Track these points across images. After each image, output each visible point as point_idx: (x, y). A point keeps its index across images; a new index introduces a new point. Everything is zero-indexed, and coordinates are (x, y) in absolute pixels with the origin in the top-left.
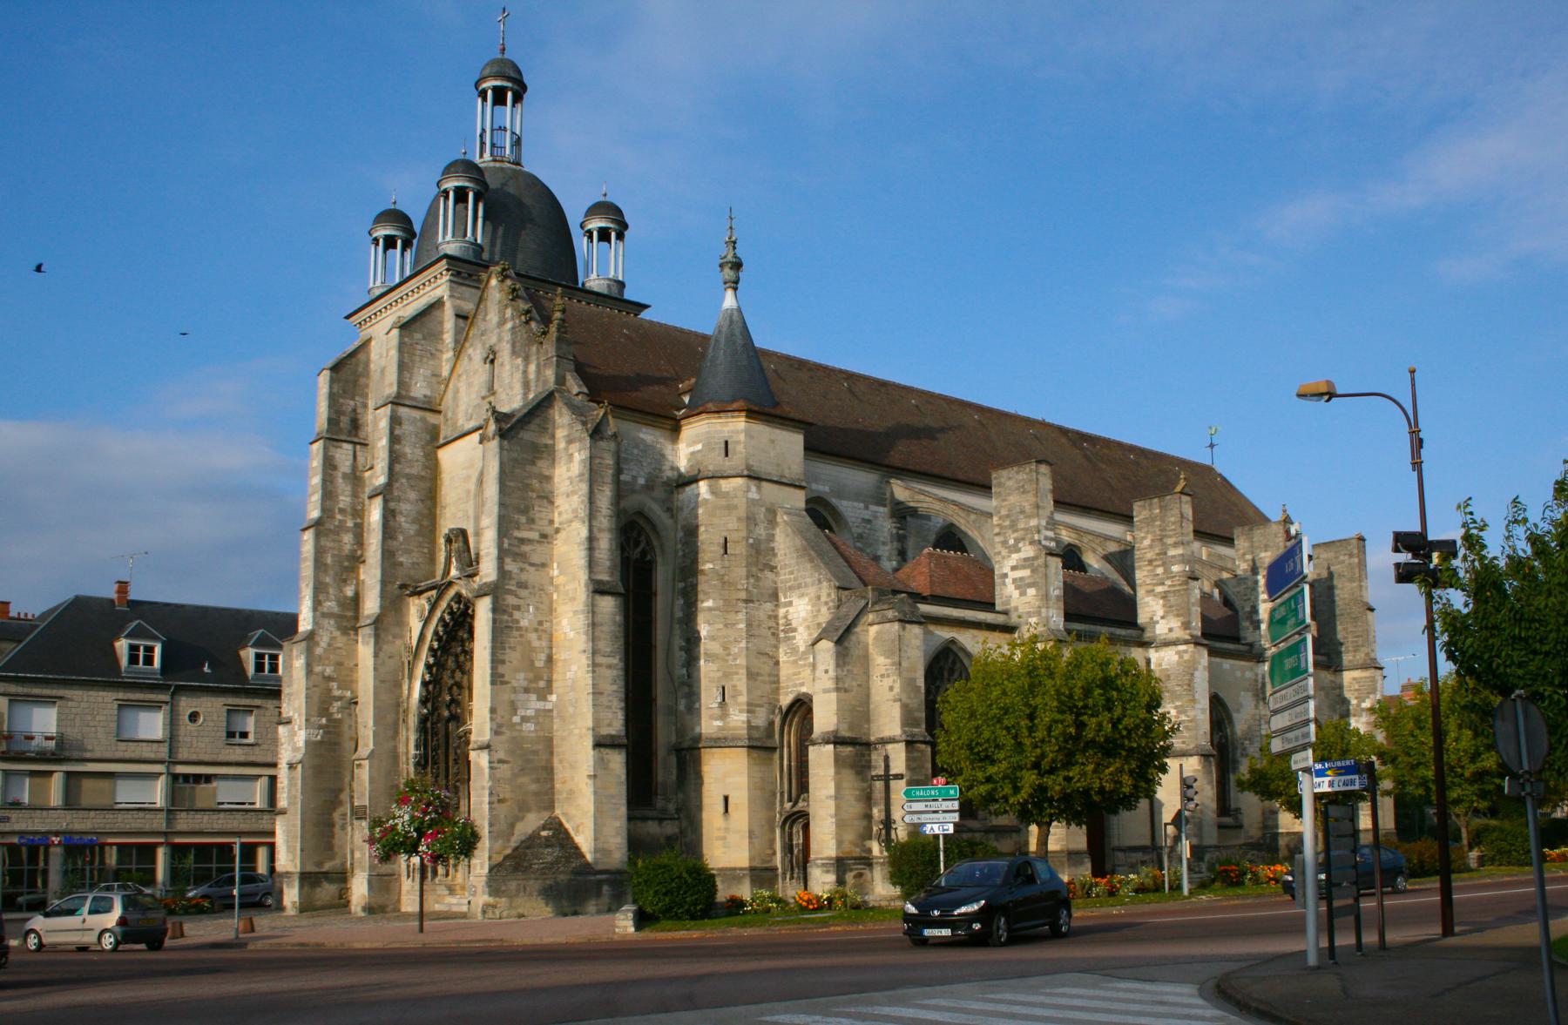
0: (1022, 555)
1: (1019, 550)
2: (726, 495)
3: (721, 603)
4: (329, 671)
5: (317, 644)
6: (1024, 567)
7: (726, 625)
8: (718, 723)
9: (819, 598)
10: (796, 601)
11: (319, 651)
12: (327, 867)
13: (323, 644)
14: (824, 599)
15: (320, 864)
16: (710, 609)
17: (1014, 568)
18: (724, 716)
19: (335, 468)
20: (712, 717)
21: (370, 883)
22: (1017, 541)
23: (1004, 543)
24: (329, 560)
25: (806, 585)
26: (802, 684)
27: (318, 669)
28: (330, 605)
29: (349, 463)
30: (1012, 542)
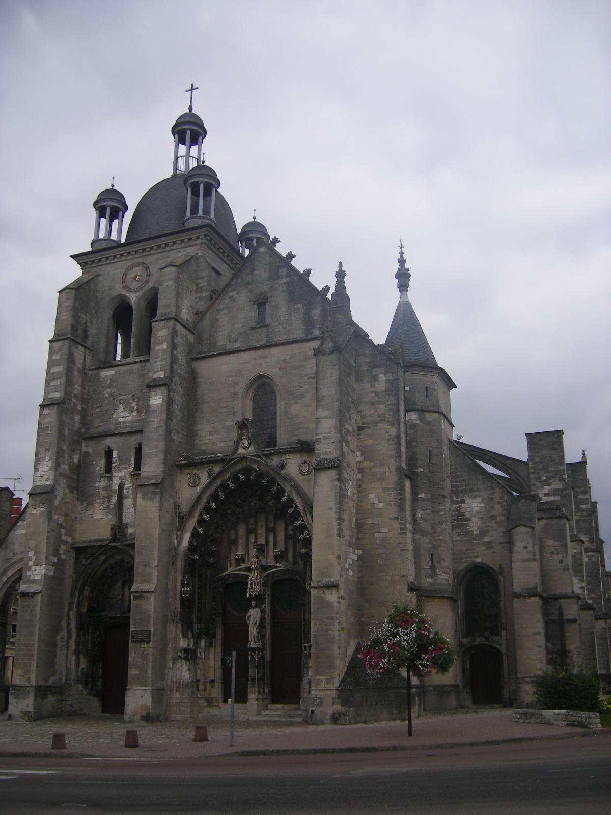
0: (553, 487)
1: (550, 484)
2: (429, 423)
3: (429, 496)
4: (61, 519)
5: (56, 497)
6: (555, 495)
7: (433, 512)
8: (430, 580)
9: (492, 499)
10: (468, 500)
11: (56, 502)
12: (51, 681)
13: (59, 498)
14: (497, 499)
15: (46, 679)
16: (422, 499)
17: (546, 495)
18: (433, 575)
19: (74, 363)
20: (427, 576)
21: (153, 696)
22: (548, 478)
23: (538, 479)
24: (66, 433)
25: (478, 490)
26: (477, 557)
27: (55, 517)
28: (65, 467)
29: (81, 361)
30: (544, 478)
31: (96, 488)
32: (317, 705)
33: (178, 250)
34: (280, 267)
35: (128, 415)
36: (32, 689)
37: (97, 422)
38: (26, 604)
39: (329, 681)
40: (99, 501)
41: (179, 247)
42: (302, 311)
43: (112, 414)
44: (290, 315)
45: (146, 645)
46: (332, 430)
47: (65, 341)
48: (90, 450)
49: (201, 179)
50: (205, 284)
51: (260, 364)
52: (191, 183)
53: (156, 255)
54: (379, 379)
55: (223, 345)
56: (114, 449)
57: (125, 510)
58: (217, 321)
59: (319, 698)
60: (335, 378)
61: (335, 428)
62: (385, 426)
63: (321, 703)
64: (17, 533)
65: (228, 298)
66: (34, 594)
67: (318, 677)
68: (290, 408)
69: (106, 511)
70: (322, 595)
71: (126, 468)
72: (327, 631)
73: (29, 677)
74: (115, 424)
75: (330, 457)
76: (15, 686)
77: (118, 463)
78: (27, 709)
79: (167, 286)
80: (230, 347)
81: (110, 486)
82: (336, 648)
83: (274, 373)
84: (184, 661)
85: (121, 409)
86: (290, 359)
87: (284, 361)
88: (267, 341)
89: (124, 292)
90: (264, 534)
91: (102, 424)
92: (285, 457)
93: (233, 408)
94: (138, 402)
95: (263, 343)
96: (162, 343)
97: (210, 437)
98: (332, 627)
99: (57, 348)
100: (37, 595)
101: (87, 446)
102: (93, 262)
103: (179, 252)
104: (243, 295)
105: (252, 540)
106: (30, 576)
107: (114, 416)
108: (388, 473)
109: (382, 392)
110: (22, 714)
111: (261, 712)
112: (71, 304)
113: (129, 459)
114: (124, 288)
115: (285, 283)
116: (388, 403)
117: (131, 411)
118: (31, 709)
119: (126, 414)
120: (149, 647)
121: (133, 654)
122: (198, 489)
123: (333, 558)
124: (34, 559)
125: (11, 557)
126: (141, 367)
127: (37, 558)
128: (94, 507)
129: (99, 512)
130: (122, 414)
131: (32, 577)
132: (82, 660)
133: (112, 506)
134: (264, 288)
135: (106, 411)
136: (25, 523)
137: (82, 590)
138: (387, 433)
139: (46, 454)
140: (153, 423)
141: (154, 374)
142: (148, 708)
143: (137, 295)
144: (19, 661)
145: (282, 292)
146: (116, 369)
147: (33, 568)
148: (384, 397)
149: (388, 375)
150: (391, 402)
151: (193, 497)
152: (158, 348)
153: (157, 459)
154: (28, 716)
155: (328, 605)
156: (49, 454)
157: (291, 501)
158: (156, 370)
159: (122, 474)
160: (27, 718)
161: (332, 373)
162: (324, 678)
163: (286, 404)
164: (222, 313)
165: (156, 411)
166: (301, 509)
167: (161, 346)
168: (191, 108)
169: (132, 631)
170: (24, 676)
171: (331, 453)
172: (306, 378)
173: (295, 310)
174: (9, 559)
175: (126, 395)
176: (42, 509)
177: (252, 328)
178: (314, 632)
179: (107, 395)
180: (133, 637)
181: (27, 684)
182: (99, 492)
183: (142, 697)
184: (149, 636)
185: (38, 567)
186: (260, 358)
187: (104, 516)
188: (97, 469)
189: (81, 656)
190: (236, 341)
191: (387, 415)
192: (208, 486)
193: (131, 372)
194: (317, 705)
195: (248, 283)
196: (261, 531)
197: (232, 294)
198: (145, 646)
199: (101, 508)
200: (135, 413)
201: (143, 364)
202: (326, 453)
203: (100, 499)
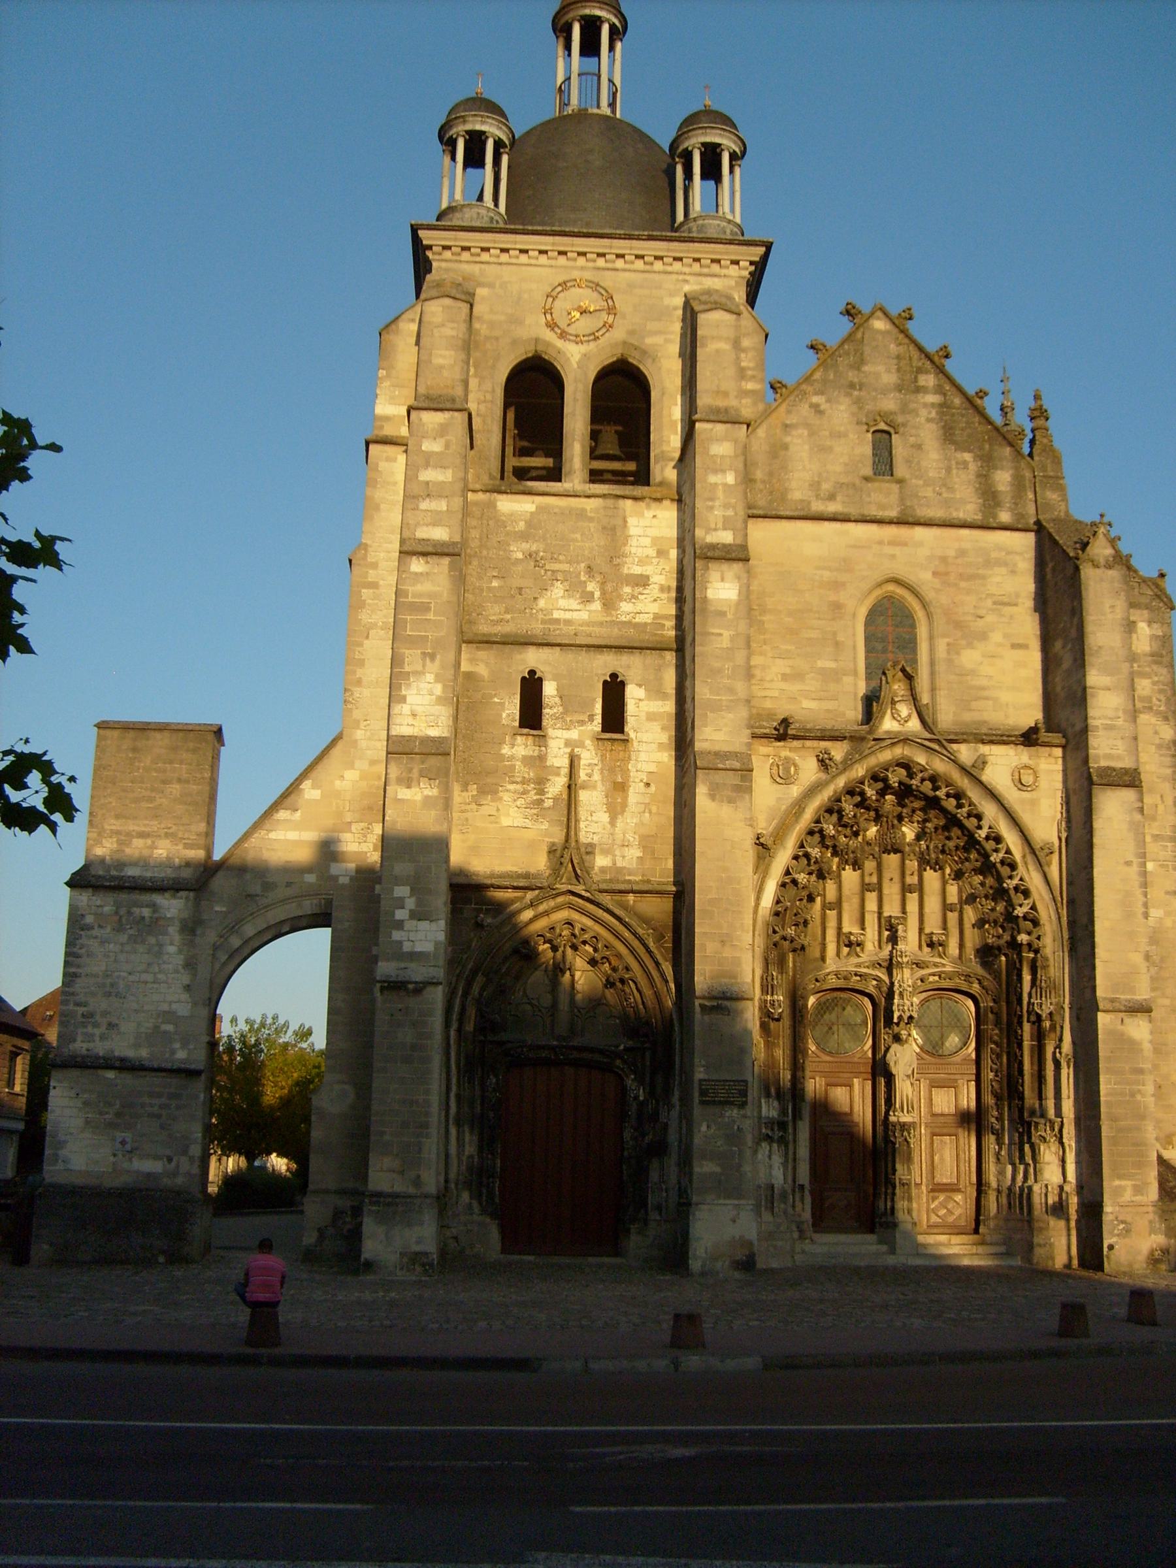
31: (502, 758)
32: (1118, 1235)
33: (681, 277)
34: (919, 371)
35: (578, 607)
36: (428, 1201)
37: (494, 611)
38: (400, 1006)
39: (1138, 1190)
40: (512, 787)
41: (687, 270)
42: (973, 467)
43: (535, 599)
44: (949, 470)
45: (735, 1111)
46: (1120, 714)
47: (456, 414)
48: (482, 670)
50: (751, 365)
51: (893, 556)
52: (703, 144)
53: (627, 274)
54: (1139, 631)
55: (802, 501)
56: (627, 679)
57: (583, 814)
58: (785, 447)
59: (1122, 1222)
60: (1119, 616)
61: (1125, 711)
62: (1153, 720)
63: (1128, 1231)
64: (273, 835)
65: (807, 406)
66: (420, 988)
67: (1117, 1183)
68: (958, 653)
69: (535, 811)
70: (1120, 1027)
71: (582, 723)
72: (1133, 1095)
73: (419, 1177)
74: (544, 622)
75: (1118, 765)
76: (379, 1194)
77: (561, 709)
79: (717, 351)
80: (817, 507)
81: (542, 758)
82: (1150, 1128)
83: (924, 578)
84: (775, 1145)
85: (558, 590)
86: (956, 558)
87: (944, 559)
88: (902, 512)
89: (549, 336)
90: (897, 898)
91: (508, 617)
92: (985, 749)
93: (835, 634)
94: (603, 584)
95: (893, 513)
96: (723, 471)
97: (783, 685)
98: (1141, 1087)
99: (430, 426)
100: (430, 989)
101: (471, 660)
103: (686, 281)
104: (842, 408)
105: (871, 905)
106: (400, 943)
107: (542, 603)
108: (1161, 808)
109: (1145, 655)
110: (405, 1260)
111: (355, 1236)
112: (461, 336)
113: (588, 704)
114: (548, 325)
115: (933, 405)
116: (1156, 679)
117: (588, 598)
118: (431, 1247)
119: (573, 604)
120: (745, 1116)
121: (704, 1128)
122: (795, 791)
123: (1137, 958)
124: (411, 903)
126: (605, 508)
127: (419, 903)
128: (501, 799)
129: (513, 811)
130: (562, 603)
131: (407, 947)
132: (467, 1137)
133: (549, 803)
134: (889, 404)
135: (521, 589)
136: (298, 814)
137: (469, 984)
138: (1156, 733)
139: (424, 666)
140: (719, 638)
141: (707, 533)
142: (751, 1243)
143: (583, 348)
144: (387, 1138)
145: (929, 420)
146: (539, 499)
147: (409, 925)
148: (1149, 666)
149: (1155, 626)
150: (1162, 678)
151: (784, 807)
152: (713, 479)
153: (731, 716)
154: (423, 1265)
155: (1132, 1046)
156: (433, 667)
158: (713, 526)
159: (574, 734)
160: (418, 1268)
161: (1113, 607)
162: (1129, 1183)
163: (948, 644)
164: (794, 433)
165: (723, 614)
166: (1017, 855)
167: (719, 476)
169: (700, 1080)
170: (402, 1173)
171: (1119, 757)
172: (989, 603)
173: (957, 463)
174: (251, 897)
175: (569, 562)
176: (428, 792)
177: (866, 479)
178: (1106, 1095)
179: (520, 556)
180: (703, 1093)
181: (412, 1190)
182: (513, 767)
183: (734, 1221)
184: (744, 1093)
185: (424, 925)
186: (893, 543)
187: (528, 823)
188: (504, 715)
189: (466, 1129)
190: (832, 497)
191: (1154, 699)
192: (813, 790)
193: (581, 514)
194: (1118, 1235)
195: (852, 386)
196: (892, 890)
197: (815, 399)
198: (734, 1112)
199: (518, 803)
200: (597, 606)
201: (610, 502)
202: (1108, 757)
203: (517, 783)
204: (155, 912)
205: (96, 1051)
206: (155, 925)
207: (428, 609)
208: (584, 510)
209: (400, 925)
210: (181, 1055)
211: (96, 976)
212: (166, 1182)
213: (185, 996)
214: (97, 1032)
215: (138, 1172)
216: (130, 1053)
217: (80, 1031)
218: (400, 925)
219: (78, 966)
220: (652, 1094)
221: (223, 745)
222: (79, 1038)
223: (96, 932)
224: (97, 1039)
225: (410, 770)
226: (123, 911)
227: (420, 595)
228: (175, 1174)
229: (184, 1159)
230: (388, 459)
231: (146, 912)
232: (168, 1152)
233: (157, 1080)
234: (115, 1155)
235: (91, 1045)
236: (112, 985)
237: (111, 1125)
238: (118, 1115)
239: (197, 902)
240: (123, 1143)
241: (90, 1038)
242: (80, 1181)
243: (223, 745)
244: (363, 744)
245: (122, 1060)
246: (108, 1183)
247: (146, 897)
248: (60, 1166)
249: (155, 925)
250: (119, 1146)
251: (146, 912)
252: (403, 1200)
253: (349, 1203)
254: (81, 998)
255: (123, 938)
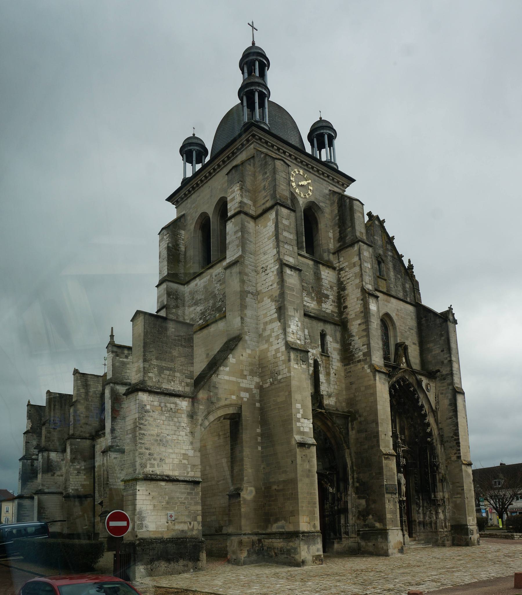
49: (325, 131)
76: (303, 533)
78: (317, 554)
102: (266, 142)
125: (216, 401)
144: (304, 508)
157: (422, 406)
168: (253, 43)
180: (387, 489)
181: (313, 530)
204: (176, 406)
205: (156, 472)
206: (175, 412)
207: (294, 291)
208: (308, 264)
209: (298, 420)
210: (191, 474)
211: (152, 435)
212: (189, 534)
213: (190, 447)
214: (156, 463)
215: (177, 530)
216: (170, 473)
217: (148, 462)
218: (298, 420)
219: (145, 430)
220: (338, 490)
221: (457, 324)
222: (148, 466)
223: (151, 414)
224: (156, 466)
225: (297, 356)
226: (162, 405)
227: (291, 284)
228: (192, 529)
229: (195, 523)
230: (247, 222)
231: (172, 406)
232: (189, 520)
233: (182, 486)
234: (167, 522)
235: (153, 469)
236: (160, 440)
237: (166, 508)
238: (168, 503)
239: (193, 405)
240: (171, 516)
241: (152, 465)
242: (153, 536)
243: (457, 324)
244: (249, 342)
245: (168, 476)
246: (166, 536)
247: (173, 399)
248: (145, 529)
249: (175, 412)
250: (169, 518)
251: (172, 406)
252: (312, 534)
253: (257, 538)
254: (147, 446)
255: (164, 418)
